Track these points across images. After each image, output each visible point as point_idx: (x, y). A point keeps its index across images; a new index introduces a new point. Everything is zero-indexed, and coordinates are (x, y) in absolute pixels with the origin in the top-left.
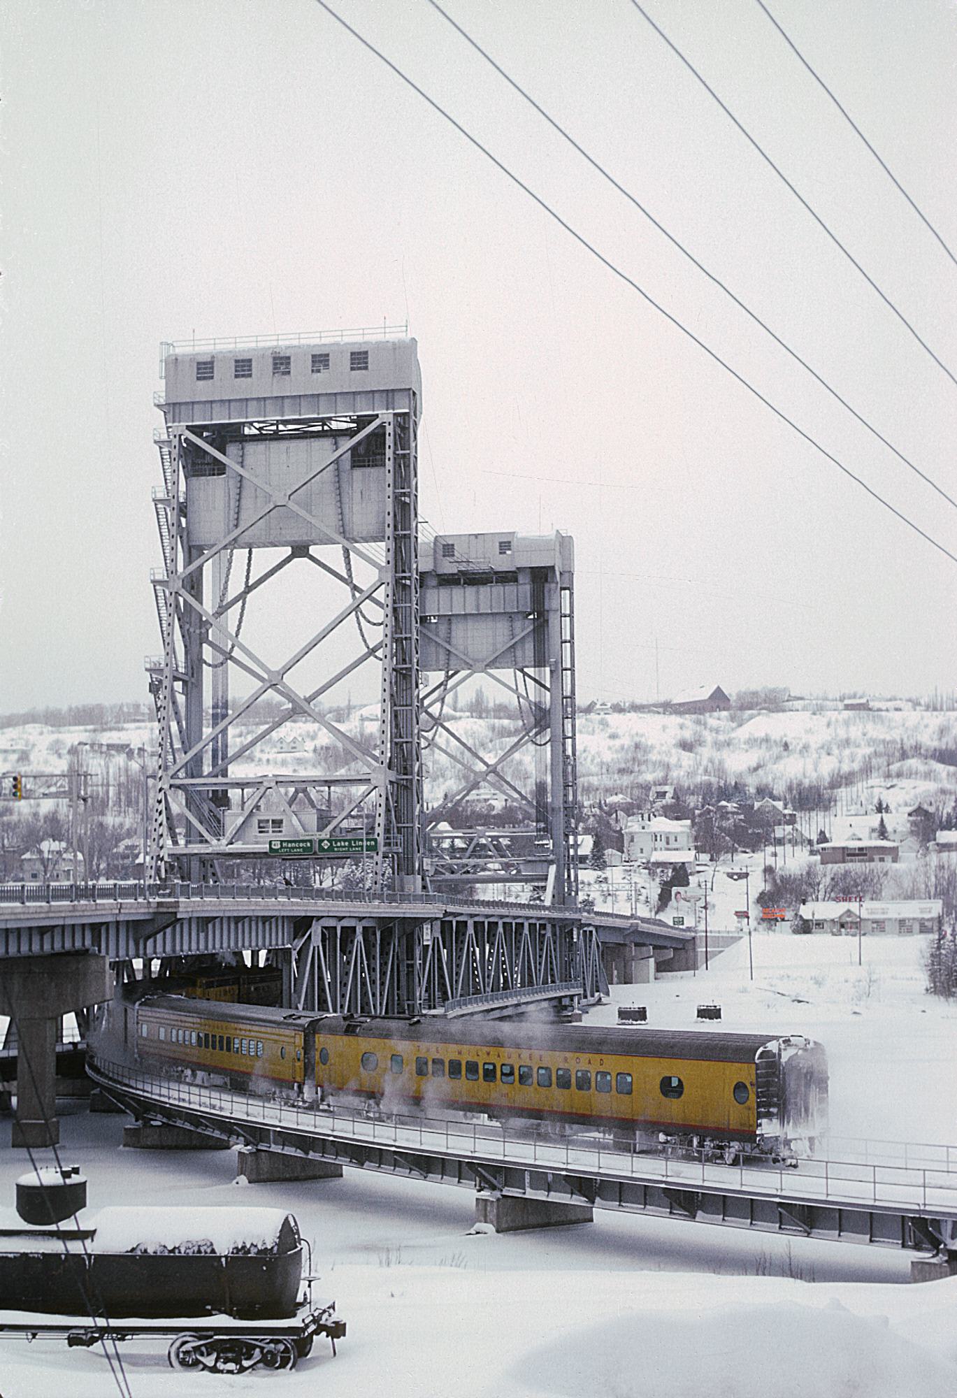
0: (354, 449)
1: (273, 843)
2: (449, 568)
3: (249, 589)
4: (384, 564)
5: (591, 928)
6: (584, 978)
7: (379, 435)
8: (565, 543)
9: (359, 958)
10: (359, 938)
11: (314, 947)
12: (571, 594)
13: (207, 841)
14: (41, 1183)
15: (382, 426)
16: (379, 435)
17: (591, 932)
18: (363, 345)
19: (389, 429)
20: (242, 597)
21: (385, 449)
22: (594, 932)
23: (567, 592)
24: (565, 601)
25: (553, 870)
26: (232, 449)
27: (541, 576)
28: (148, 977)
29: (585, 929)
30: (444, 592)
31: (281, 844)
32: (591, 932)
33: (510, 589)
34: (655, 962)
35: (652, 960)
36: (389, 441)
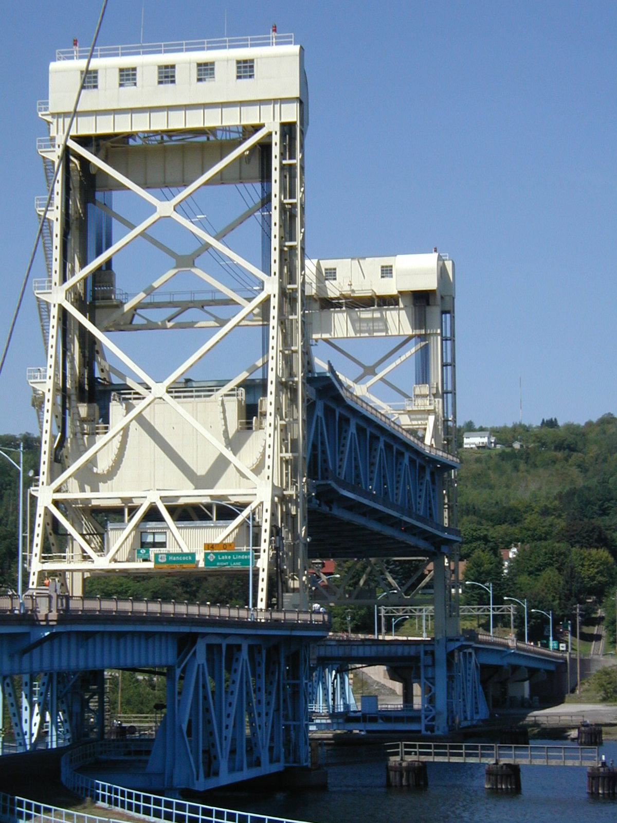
1: (160, 556)
5: (470, 650)
6: (464, 700)
7: (264, 148)
9: (245, 677)
10: (245, 654)
11: (199, 665)
12: (453, 318)
13: (89, 557)
14: (101, 608)
15: (269, 135)
16: (264, 148)
17: (470, 654)
18: (219, 134)
23: (448, 315)
24: (446, 324)
28: (112, 387)
29: (465, 651)
31: (167, 558)
32: (470, 654)
34: (530, 684)
35: (527, 684)
36: (276, 151)
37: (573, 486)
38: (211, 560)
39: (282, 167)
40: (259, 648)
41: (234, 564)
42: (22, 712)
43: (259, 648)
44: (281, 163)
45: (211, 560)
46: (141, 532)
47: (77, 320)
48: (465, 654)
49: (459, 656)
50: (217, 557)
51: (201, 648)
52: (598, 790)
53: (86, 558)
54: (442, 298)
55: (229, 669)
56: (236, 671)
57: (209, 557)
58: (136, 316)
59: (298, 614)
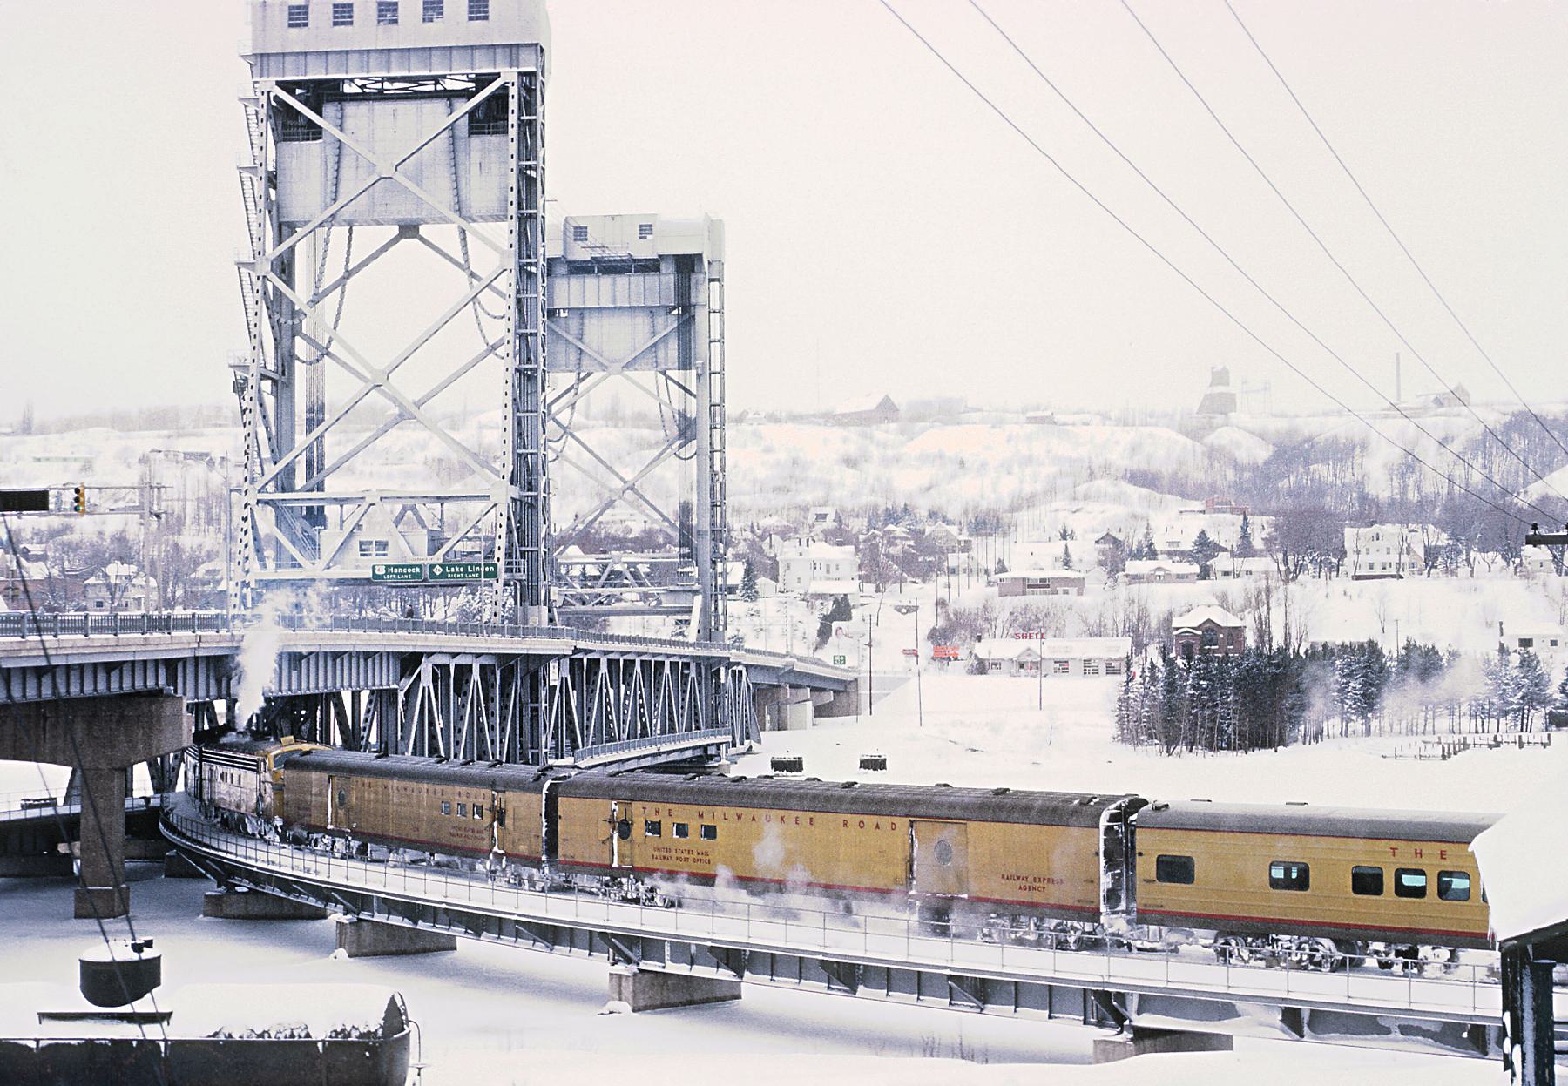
0: (472, 114)
2: (581, 254)
3: (349, 274)
4: (506, 247)
5: (740, 668)
7: (501, 97)
8: (714, 228)
12: (721, 286)
15: (504, 88)
16: (501, 97)
19: (513, 91)
20: (341, 282)
21: (507, 113)
22: (744, 673)
25: (698, 599)
26: (330, 109)
27: (687, 265)
29: (734, 668)
30: (575, 282)
31: (386, 570)
32: (740, 672)
33: (651, 279)
36: (513, 104)
37: (739, 427)
39: (521, 124)
40: (492, 668)
42: (177, 1046)
43: (492, 668)
44: (519, 119)
47: (306, 117)
48: (734, 672)
49: (727, 675)
50: (444, 569)
51: (426, 669)
52: (964, 899)
53: (296, 565)
54: (709, 263)
55: (457, 692)
56: (466, 694)
58: (557, 418)
59: (559, 660)
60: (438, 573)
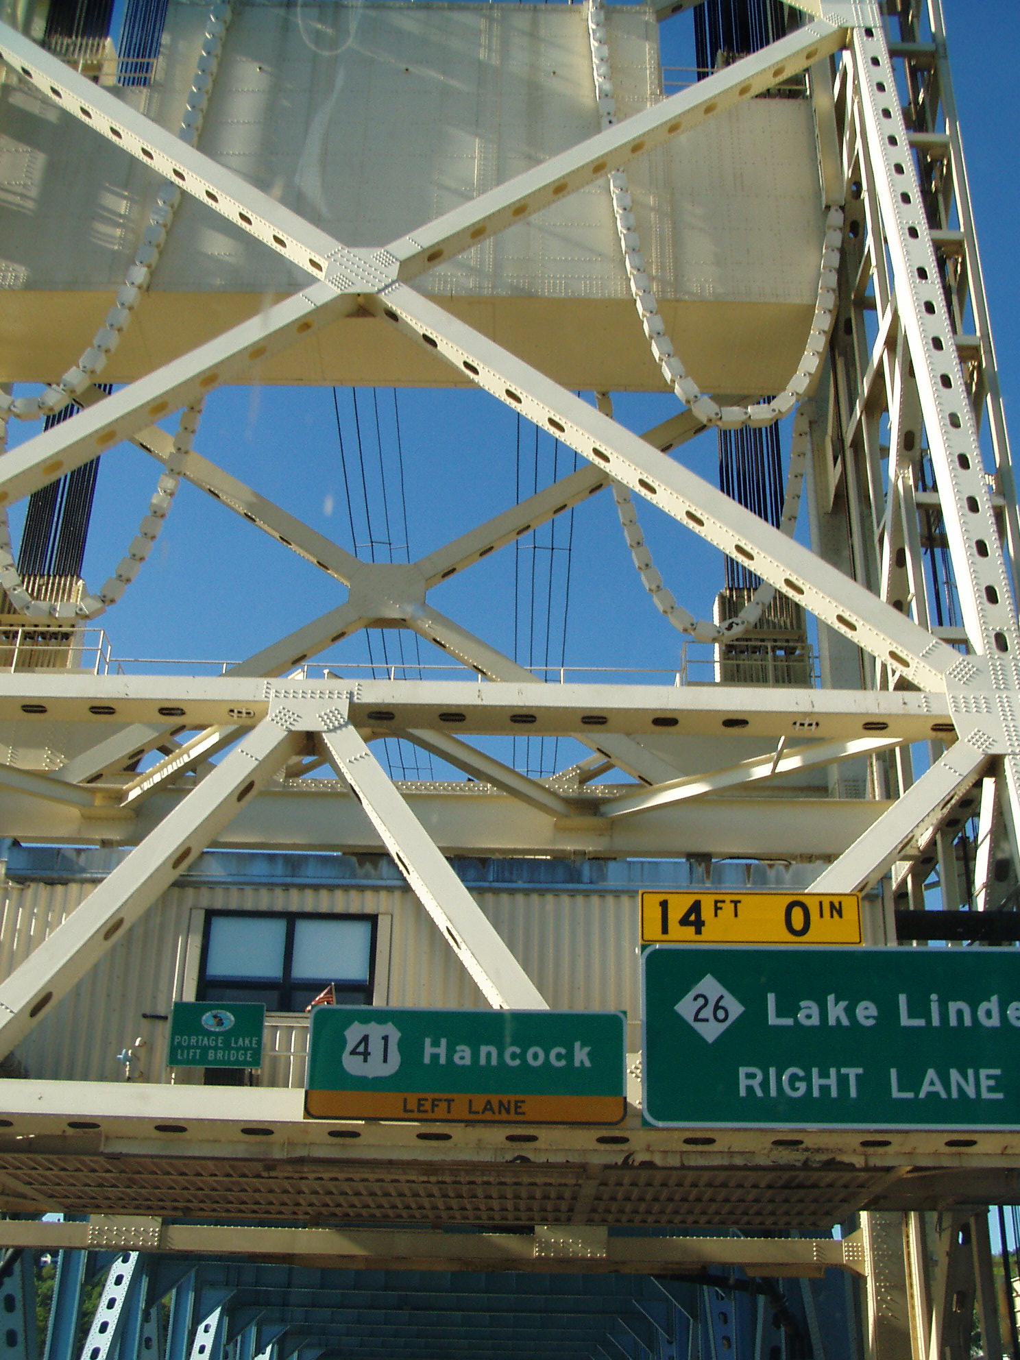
31: (410, 1049)
38: (710, 1031)
41: (931, 1082)
45: (710, 1031)
46: (373, 919)
57: (686, 1008)
60: (710, 986)
